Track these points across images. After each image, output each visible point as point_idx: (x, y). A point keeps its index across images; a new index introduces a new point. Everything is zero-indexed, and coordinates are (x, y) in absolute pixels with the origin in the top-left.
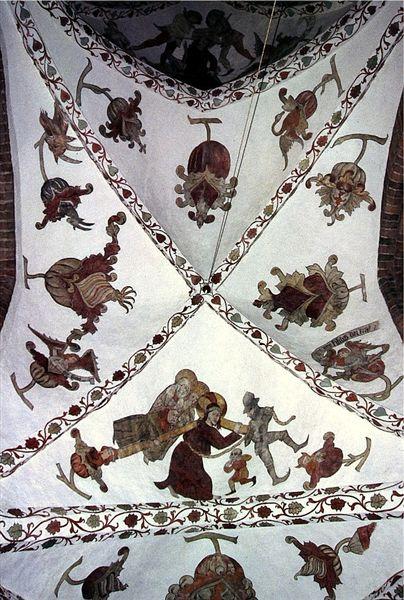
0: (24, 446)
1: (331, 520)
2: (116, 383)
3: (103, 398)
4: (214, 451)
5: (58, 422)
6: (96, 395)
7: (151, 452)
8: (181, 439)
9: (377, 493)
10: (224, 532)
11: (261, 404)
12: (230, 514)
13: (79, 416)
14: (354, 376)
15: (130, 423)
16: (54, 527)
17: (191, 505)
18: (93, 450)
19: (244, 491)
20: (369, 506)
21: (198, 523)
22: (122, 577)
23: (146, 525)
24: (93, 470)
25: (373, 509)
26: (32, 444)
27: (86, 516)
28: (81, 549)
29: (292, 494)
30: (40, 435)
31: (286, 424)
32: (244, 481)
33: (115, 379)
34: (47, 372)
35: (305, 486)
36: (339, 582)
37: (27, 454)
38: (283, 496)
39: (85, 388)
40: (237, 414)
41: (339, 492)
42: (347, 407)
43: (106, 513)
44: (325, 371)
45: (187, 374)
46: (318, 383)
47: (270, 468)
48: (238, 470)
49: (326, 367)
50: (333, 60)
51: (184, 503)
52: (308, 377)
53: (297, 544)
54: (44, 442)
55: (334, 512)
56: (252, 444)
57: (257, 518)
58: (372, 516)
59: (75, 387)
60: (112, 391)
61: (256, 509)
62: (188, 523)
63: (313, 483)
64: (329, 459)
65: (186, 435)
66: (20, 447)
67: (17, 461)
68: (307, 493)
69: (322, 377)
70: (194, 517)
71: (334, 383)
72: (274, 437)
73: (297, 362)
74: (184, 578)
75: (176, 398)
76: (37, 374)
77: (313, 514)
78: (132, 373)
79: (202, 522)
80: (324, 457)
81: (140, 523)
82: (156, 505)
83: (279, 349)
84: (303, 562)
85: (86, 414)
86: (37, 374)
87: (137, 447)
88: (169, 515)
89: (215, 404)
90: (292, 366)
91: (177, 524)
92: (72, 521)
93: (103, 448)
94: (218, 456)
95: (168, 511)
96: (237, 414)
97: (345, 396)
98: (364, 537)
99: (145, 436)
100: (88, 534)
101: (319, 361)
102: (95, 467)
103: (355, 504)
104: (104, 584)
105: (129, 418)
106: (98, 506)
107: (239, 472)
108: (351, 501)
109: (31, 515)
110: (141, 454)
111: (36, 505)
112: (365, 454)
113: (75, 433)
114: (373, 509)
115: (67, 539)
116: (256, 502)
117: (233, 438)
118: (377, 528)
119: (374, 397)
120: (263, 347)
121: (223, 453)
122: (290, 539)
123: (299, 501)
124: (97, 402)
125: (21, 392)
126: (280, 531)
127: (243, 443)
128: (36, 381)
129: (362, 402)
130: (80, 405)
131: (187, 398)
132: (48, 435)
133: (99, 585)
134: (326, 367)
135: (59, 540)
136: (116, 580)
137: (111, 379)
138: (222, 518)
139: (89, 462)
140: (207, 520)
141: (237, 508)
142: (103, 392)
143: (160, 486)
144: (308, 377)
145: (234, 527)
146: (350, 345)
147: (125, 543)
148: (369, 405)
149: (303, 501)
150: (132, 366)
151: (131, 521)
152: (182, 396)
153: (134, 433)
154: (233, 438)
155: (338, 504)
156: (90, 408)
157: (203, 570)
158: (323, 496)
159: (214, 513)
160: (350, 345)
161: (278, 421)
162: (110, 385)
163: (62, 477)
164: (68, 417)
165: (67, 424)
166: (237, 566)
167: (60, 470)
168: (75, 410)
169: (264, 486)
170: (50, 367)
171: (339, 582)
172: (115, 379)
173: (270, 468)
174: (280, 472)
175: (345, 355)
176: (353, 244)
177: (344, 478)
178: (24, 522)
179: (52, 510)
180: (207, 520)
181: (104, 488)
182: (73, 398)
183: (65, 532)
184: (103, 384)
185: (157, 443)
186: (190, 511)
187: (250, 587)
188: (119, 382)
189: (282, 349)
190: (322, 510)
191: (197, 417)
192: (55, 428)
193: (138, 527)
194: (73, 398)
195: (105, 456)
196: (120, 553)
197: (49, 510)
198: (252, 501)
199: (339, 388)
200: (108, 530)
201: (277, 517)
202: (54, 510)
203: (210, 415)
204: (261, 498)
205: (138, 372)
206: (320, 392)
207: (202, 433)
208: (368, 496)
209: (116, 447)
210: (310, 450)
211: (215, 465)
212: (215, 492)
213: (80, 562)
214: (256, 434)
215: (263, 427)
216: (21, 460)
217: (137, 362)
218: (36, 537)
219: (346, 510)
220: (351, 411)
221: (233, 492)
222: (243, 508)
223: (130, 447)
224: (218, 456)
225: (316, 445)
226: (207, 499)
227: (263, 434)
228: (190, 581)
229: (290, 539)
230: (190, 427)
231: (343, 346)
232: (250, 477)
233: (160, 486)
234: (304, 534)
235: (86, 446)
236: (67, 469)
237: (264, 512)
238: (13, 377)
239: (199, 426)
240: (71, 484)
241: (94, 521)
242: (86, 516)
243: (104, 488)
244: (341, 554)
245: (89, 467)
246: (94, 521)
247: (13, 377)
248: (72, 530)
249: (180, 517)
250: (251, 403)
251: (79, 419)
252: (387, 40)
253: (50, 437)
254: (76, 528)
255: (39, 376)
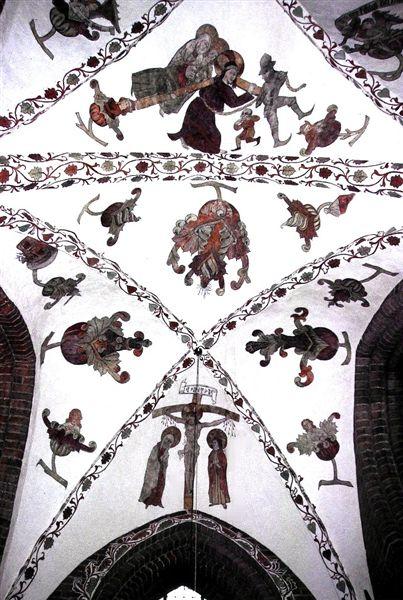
0: (43, 96)
1: (318, 185)
2: (135, 35)
3: (122, 50)
4: (227, 108)
5: (77, 73)
6: (114, 47)
7: (167, 106)
8: (197, 94)
9: (360, 169)
10: (225, 182)
11: (276, 68)
12: (231, 168)
13: (97, 68)
14: (372, 50)
15: (147, 77)
16: (72, 170)
17: (198, 156)
18: (112, 100)
19: (248, 149)
20: (351, 179)
21: (203, 173)
22: (136, 212)
23: (155, 171)
24: (110, 119)
25: (354, 183)
26: (51, 94)
27: (101, 161)
28: (96, 187)
29: (288, 158)
30: (58, 86)
31: (296, 90)
32: (249, 140)
33: (134, 31)
34: (67, 20)
35: (301, 153)
36: (316, 235)
37: (47, 104)
38: (280, 158)
39: (105, 38)
40: (253, 75)
41: (329, 163)
42: (355, 82)
43: (120, 159)
44: (345, 41)
45: (208, 30)
46: (333, 54)
47: (274, 131)
48: (246, 129)
49: (347, 36)
50: (348, 484)
51: (192, 155)
52: (324, 47)
53: (287, 200)
54: (63, 92)
55: (321, 179)
56: (263, 106)
57: (254, 175)
58: (352, 188)
59: (95, 37)
60: (130, 43)
61: (254, 167)
62: (194, 172)
63: (308, 151)
64: (328, 131)
65: (202, 91)
66: (39, 97)
67: (37, 111)
68: (302, 158)
69: (338, 49)
70: (200, 167)
71: (348, 56)
72: (283, 102)
73: (317, 29)
74: (190, 216)
75: (195, 54)
76: (58, 21)
77: (303, 178)
78: (152, 25)
79: (206, 172)
80: (323, 128)
81: (150, 169)
82: (166, 155)
83: (301, 11)
84: (289, 215)
85: (104, 65)
86: (58, 21)
87: (154, 99)
88: (177, 164)
89: (233, 63)
90: (311, 33)
91: (185, 173)
92: (87, 165)
93: (121, 100)
94: (229, 113)
95: (177, 161)
96: (253, 75)
97: (355, 71)
98: (343, 203)
99: (162, 89)
100: (102, 177)
101: (340, 29)
102: (113, 117)
103: (340, 175)
104: (120, 216)
105: (147, 71)
106: (113, 153)
107: (247, 131)
108: (338, 172)
109: (50, 159)
110: (157, 107)
111: (56, 152)
112: (361, 131)
113: (94, 84)
114: (354, 183)
115: (84, 180)
116: (255, 161)
117: (246, 98)
118: (355, 197)
119: (384, 76)
120: (287, 8)
121: (236, 111)
122: (281, 195)
123: (293, 165)
124: (115, 55)
125: (41, 40)
126: (273, 187)
127: (254, 104)
128: (56, 453)
129: (369, 81)
130: (98, 57)
131: (206, 55)
132: (66, 85)
133: (116, 217)
134: (347, 36)
135: (77, 181)
136: (130, 214)
137: (129, 31)
138: (224, 171)
139: (108, 111)
140: (211, 171)
141: (239, 164)
142: (122, 44)
143: (173, 137)
144: (324, 47)
145: (235, 179)
146: (378, 15)
147: (136, 185)
148: (376, 84)
149: (295, 165)
150: (152, 18)
151: (142, 167)
152: (201, 52)
153: (152, 86)
154: (246, 98)
155: (325, 173)
156: (108, 61)
157: (205, 211)
158: (315, 164)
159: (214, 169)
160: (378, 15)
161: (289, 87)
162: (128, 38)
163: (81, 125)
164: (87, 68)
165: (85, 76)
166: (235, 211)
167: (80, 118)
168: (93, 62)
169: (266, 147)
170: (70, 14)
171: (316, 235)
172: (134, 31)
173: (274, 131)
174: (282, 136)
175: (369, 26)
176: (60, 386)
177: (336, 150)
178: (43, 166)
179: (70, 156)
180: (211, 171)
181: (120, 137)
182: (93, 48)
183: (81, 174)
184: (121, 36)
185: (174, 97)
186: (197, 162)
187: (244, 229)
188: (138, 34)
189: (305, 13)
190: (311, 176)
191: (214, 74)
192: (73, 80)
193: (148, 173)
194: (93, 48)
195: (123, 107)
196: (133, 193)
197: (67, 155)
198: (252, 159)
199: (352, 62)
200: (121, 174)
201: (272, 176)
202: (72, 155)
203: (227, 73)
204: (262, 158)
205: (158, 24)
206: (333, 64)
207: (218, 91)
208: (353, 171)
209: (134, 98)
210: (313, 119)
211: (226, 122)
212: (223, 147)
213: (98, 198)
214: (268, 97)
215: (275, 91)
216: (41, 110)
217: (157, 13)
218: (55, 178)
219: (332, 178)
220: (358, 87)
221: (239, 148)
222: (244, 164)
223: (147, 99)
224: (229, 113)
225: (319, 116)
226: (214, 153)
227: (275, 97)
228: (194, 219)
229: (281, 195)
230: (206, 84)
231: (369, 15)
232: (256, 137)
233: (173, 137)
234: (293, 193)
235: (104, 97)
236: (86, 118)
237: (261, 170)
238: (32, 24)
239: (215, 84)
240: (89, 132)
241: (108, 166)
242: (101, 161)
243: (120, 137)
244: (323, 215)
245: (107, 117)
246: (108, 166)
247: (41, 462)
248: (88, 173)
249: (187, 167)
250: (268, 65)
251: (97, 71)
252: (313, 172)
253: (68, 88)
254: (91, 171)
255: (59, 24)
